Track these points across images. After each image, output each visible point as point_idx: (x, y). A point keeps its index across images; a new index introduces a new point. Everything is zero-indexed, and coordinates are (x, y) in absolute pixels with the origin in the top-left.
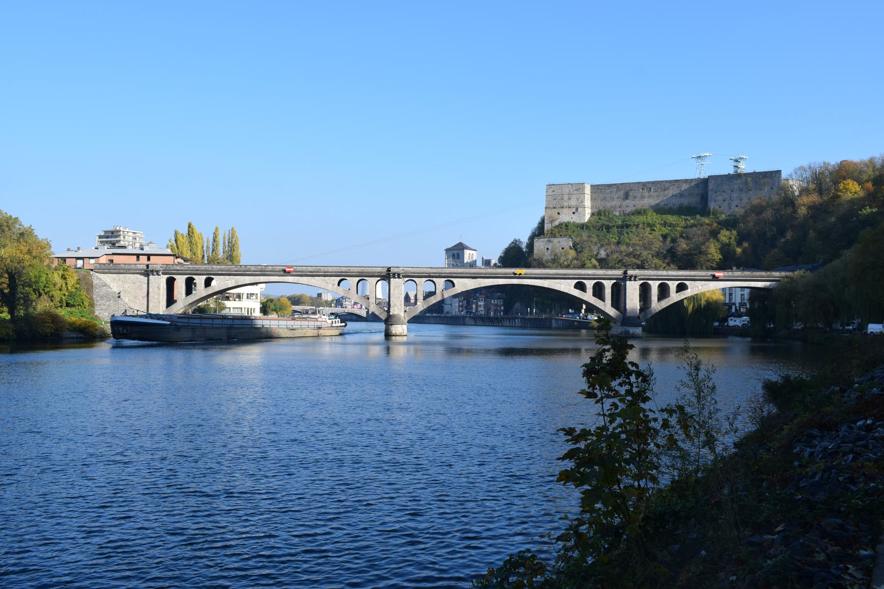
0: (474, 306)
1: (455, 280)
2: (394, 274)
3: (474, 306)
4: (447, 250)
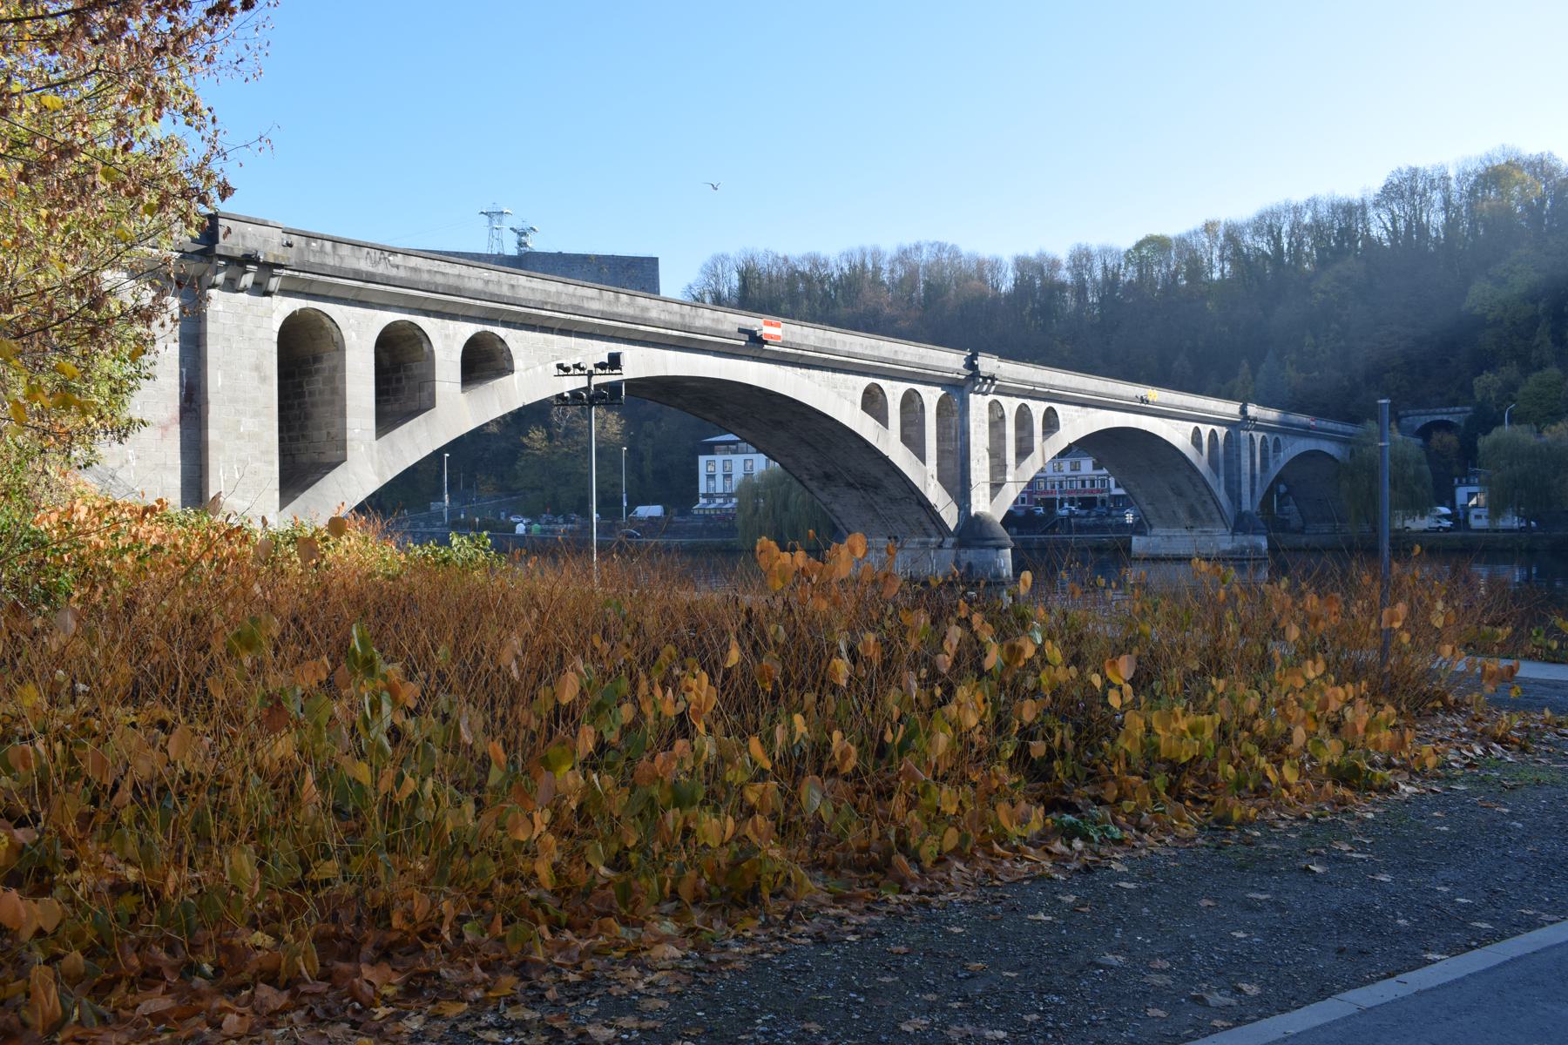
4: (653, 262)
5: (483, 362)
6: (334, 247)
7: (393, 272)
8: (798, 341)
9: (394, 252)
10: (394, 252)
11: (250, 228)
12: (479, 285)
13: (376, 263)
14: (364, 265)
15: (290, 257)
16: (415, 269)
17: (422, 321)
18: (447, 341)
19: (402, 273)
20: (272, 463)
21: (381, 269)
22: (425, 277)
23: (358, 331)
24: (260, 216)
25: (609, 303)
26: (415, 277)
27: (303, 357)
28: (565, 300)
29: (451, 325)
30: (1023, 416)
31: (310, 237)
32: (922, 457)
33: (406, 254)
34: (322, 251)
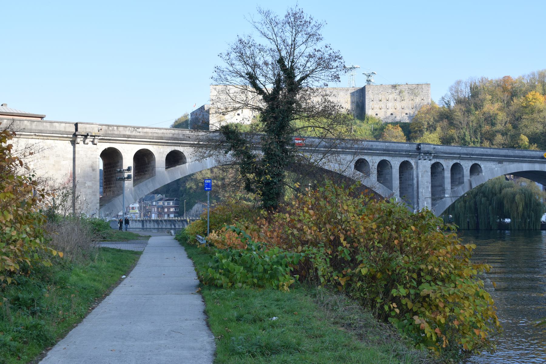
1: (483, 165)
2: (86, 136)
5: (475, 169)
6: (117, 128)
7: (138, 134)
8: (395, 148)
9: (138, 128)
10: (138, 128)
11: (88, 126)
12: (171, 135)
13: (132, 132)
14: (128, 133)
15: (101, 133)
16: (146, 133)
17: (366, 158)
18: (466, 165)
19: (141, 134)
20: (428, 187)
21: (134, 133)
22: (150, 135)
23: (447, 165)
24: (94, 122)
26: (146, 135)
27: (436, 169)
28: (448, 151)
29: (466, 162)
30: (456, 168)
31: (109, 126)
32: (390, 188)
33: (143, 128)
34: (113, 130)
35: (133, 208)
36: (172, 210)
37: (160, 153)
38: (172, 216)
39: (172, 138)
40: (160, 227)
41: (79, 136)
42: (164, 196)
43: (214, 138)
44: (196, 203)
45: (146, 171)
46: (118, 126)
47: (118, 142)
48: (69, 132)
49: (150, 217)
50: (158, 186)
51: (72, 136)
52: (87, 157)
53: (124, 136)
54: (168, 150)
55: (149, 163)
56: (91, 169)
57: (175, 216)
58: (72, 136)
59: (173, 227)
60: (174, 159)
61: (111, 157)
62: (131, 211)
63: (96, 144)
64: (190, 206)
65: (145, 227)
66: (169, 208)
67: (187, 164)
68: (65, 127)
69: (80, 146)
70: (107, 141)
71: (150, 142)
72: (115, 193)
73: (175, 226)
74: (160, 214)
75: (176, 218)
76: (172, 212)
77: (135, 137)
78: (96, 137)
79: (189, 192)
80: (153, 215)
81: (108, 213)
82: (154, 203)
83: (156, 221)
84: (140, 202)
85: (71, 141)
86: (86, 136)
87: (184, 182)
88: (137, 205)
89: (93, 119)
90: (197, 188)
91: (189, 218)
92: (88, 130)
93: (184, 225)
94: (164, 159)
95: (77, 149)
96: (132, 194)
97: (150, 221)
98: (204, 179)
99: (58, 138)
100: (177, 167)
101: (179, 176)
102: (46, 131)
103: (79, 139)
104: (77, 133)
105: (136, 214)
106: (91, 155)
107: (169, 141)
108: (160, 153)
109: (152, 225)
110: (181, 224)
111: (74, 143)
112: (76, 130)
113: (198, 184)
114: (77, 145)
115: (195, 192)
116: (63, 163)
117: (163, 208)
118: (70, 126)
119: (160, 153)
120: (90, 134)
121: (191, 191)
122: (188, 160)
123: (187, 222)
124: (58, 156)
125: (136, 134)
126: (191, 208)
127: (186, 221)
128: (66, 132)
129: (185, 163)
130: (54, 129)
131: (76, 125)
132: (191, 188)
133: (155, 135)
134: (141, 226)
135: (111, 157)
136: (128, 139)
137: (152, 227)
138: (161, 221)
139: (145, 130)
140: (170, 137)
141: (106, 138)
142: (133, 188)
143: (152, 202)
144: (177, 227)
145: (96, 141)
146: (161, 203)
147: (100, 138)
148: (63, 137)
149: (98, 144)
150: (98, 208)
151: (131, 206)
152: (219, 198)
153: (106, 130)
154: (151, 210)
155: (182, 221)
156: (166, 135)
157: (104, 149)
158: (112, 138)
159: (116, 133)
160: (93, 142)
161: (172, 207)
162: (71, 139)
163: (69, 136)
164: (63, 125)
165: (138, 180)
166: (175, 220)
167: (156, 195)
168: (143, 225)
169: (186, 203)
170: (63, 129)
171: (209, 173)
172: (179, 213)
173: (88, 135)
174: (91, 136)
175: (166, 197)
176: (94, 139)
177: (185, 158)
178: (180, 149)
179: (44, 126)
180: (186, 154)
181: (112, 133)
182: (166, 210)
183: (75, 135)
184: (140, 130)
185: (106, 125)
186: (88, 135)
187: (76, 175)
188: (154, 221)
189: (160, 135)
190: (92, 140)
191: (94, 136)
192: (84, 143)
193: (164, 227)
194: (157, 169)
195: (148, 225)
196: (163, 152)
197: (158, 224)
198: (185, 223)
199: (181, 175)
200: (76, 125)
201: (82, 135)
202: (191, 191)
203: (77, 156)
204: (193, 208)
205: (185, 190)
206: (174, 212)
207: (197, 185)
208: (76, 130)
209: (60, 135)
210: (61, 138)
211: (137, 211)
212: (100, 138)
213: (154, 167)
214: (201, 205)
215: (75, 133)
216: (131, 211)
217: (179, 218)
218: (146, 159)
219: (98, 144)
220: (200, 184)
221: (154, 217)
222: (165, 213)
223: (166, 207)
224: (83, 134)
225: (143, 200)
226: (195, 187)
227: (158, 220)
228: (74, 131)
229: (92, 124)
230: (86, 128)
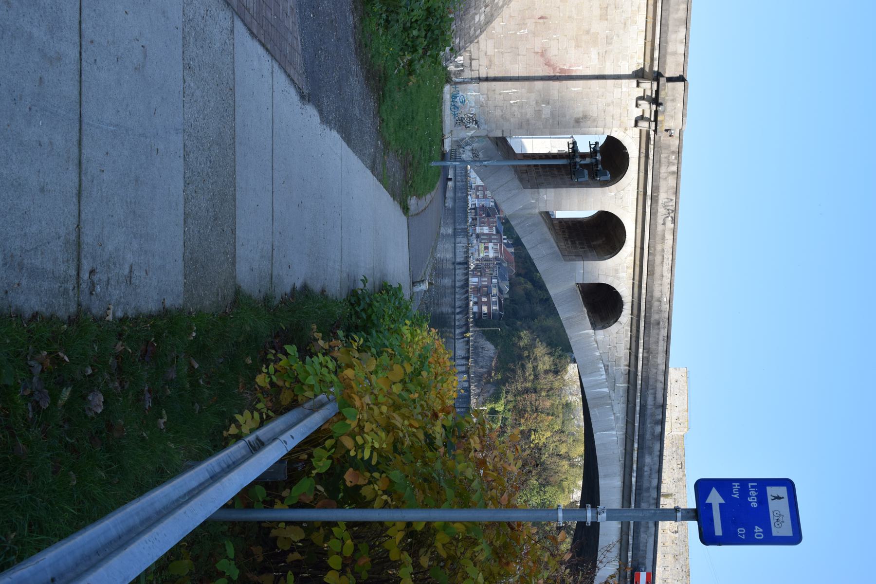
0: (486, 230)
2: (655, 101)
3: (486, 230)
6: (673, 173)
7: (660, 221)
9: (674, 221)
10: (674, 221)
11: (680, 105)
12: (657, 294)
13: (665, 206)
14: (662, 197)
15: (663, 136)
16: (663, 238)
19: (660, 228)
21: (661, 211)
22: (659, 247)
25: (653, 415)
26: (658, 238)
31: (679, 153)
34: (670, 164)
35: (486, 248)
36: (485, 309)
37: (617, 271)
38: (476, 309)
39: (652, 297)
40: (457, 290)
41: (655, 84)
42: (507, 296)
43: (651, 391)
44: (496, 347)
45: (573, 243)
46: (677, 174)
47: (642, 175)
48: (665, 63)
49: (474, 276)
50: (542, 266)
51: (656, 69)
52: (608, 105)
53: (655, 189)
54: (625, 290)
55: (593, 248)
56: (581, 115)
57: (474, 313)
58: (656, 69)
59: (458, 310)
60: (602, 303)
61: (610, 161)
62: (482, 246)
63: (636, 125)
64: (491, 337)
65: (457, 267)
66: (488, 304)
67: (592, 331)
68: (675, 53)
69: (631, 90)
70: (643, 150)
71: (642, 248)
72: (525, 176)
73: (458, 313)
74: (478, 290)
75: (471, 316)
76: (480, 309)
77: (653, 213)
78: (653, 124)
79: (513, 336)
80: (476, 280)
81: (481, 156)
82: (494, 281)
83: (466, 284)
84: (496, 258)
85: (643, 69)
86: (655, 101)
87: (529, 328)
88: (491, 254)
89: (692, 116)
90: (519, 348)
91: (472, 336)
92: (669, 106)
93: (460, 327)
94: (602, 280)
95: (625, 82)
96: (523, 209)
97: (467, 274)
98: (535, 359)
99: (649, 38)
100: (585, 310)
101: (564, 313)
102: (668, 10)
103: (647, 87)
104: (662, 80)
105: (477, 253)
106: (616, 114)
107: (644, 291)
108: (617, 271)
109: (460, 277)
110: (462, 323)
111: (639, 75)
112: (670, 80)
113: (527, 349)
114: (634, 82)
115: (514, 345)
116: (594, 54)
117: (488, 294)
118: (678, 65)
119: (617, 271)
120: (660, 108)
121: (515, 339)
122: (601, 334)
123: (466, 332)
124: (609, 40)
125: (659, 214)
126: (488, 339)
127: (467, 331)
128: (665, 56)
129: (594, 326)
130: (670, 28)
131: (681, 79)
132: (520, 338)
133: (658, 259)
134: (458, 260)
135: (610, 161)
136: (647, 197)
137: (458, 278)
138: (467, 292)
139: (669, 237)
140: (652, 291)
141: (651, 147)
142: (537, 211)
143: (496, 278)
144: (458, 317)
145: (644, 125)
146: (495, 291)
147: (652, 133)
148: (653, 50)
149: (637, 130)
150: (492, 135)
151: (490, 245)
152: (504, 385)
153: (669, 146)
154: (485, 277)
155: (467, 324)
156: (657, 283)
157: (625, 144)
158: (650, 162)
159: (663, 170)
160: (642, 118)
161: (489, 309)
162: (647, 69)
163: (656, 63)
164: (681, 50)
165: (553, 225)
166: (468, 313)
167: (507, 283)
168: (460, 263)
169: (495, 331)
170: (671, 48)
171: (545, 367)
172: (479, 320)
173: (658, 104)
174: (656, 112)
175: (505, 299)
176: (649, 120)
177: (604, 327)
178: (625, 316)
179: (678, 4)
180: (614, 328)
181: (663, 160)
182: (484, 299)
183: (657, 77)
184: (669, 225)
185: (680, 147)
186: (658, 104)
187: (565, 83)
188: (467, 280)
189: (657, 270)
190: (647, 115)
191: (656, 120)
192: (639, 99)
193: (457, 296)
194: (580, 264)
195: (460, 272)
196: (619, 278)
197: (462, 287)
198: (463, 330)
199: (567, 319)
200: (681, 79)
201: (657, 92)
202: (515, 339)
203: (610, 82)
204: (488, 343)
205: (517, 330)
206: (480, 312)
207: (525, 348)
208: (670, 80)
209: (656, 43)
210: (650, 46)
211: (482, 255)
212: (652, 133)
213: (584, 257)
214: (492, 355)
215: (663, 76)
216: (482, 246)
217: (471, 320)
218: (600, 242)
219: (637, 130)
220: (526, 353)
221: (473, 280)
222: (479, 298)
223: (489, 299)
224: (662, 94)
225: (499, 264)
226: (522, 344)
227: (468, 286)
228: (668, 74)
229: (683, 115)
230: (673, 100)
